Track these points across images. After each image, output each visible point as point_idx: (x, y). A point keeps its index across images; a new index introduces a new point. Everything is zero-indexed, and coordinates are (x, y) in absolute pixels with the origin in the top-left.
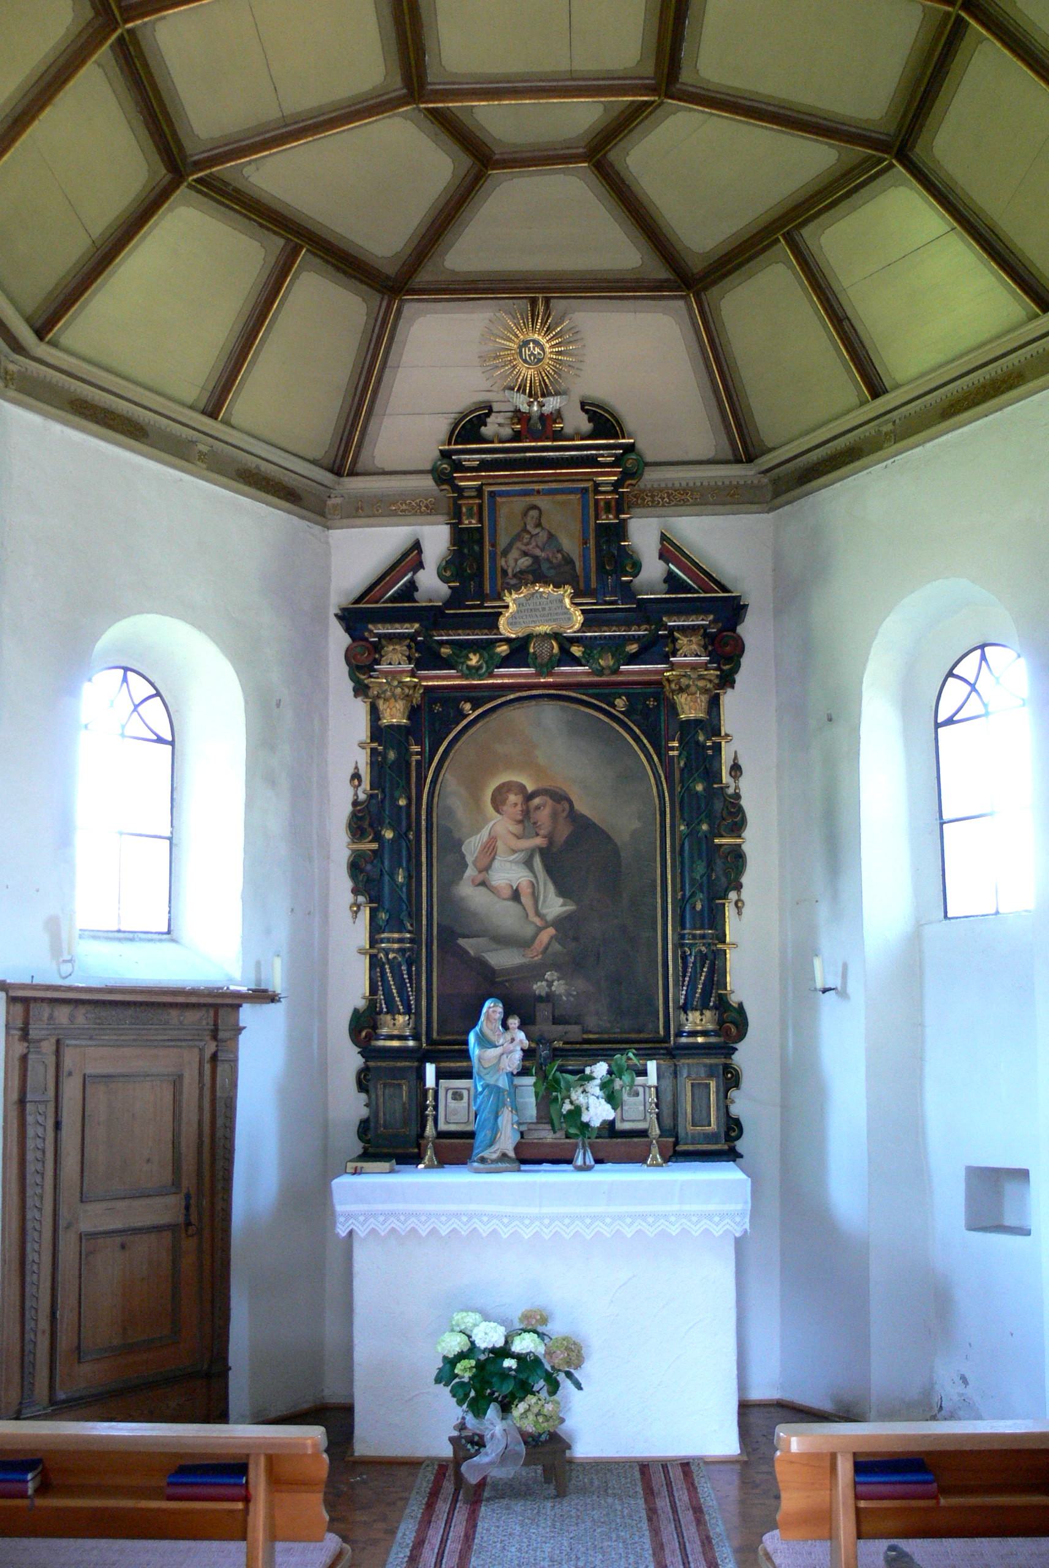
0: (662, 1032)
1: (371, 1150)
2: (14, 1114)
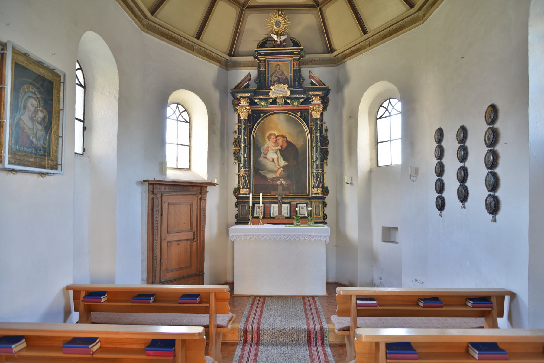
1: (238, 221)
2: (150, 211)
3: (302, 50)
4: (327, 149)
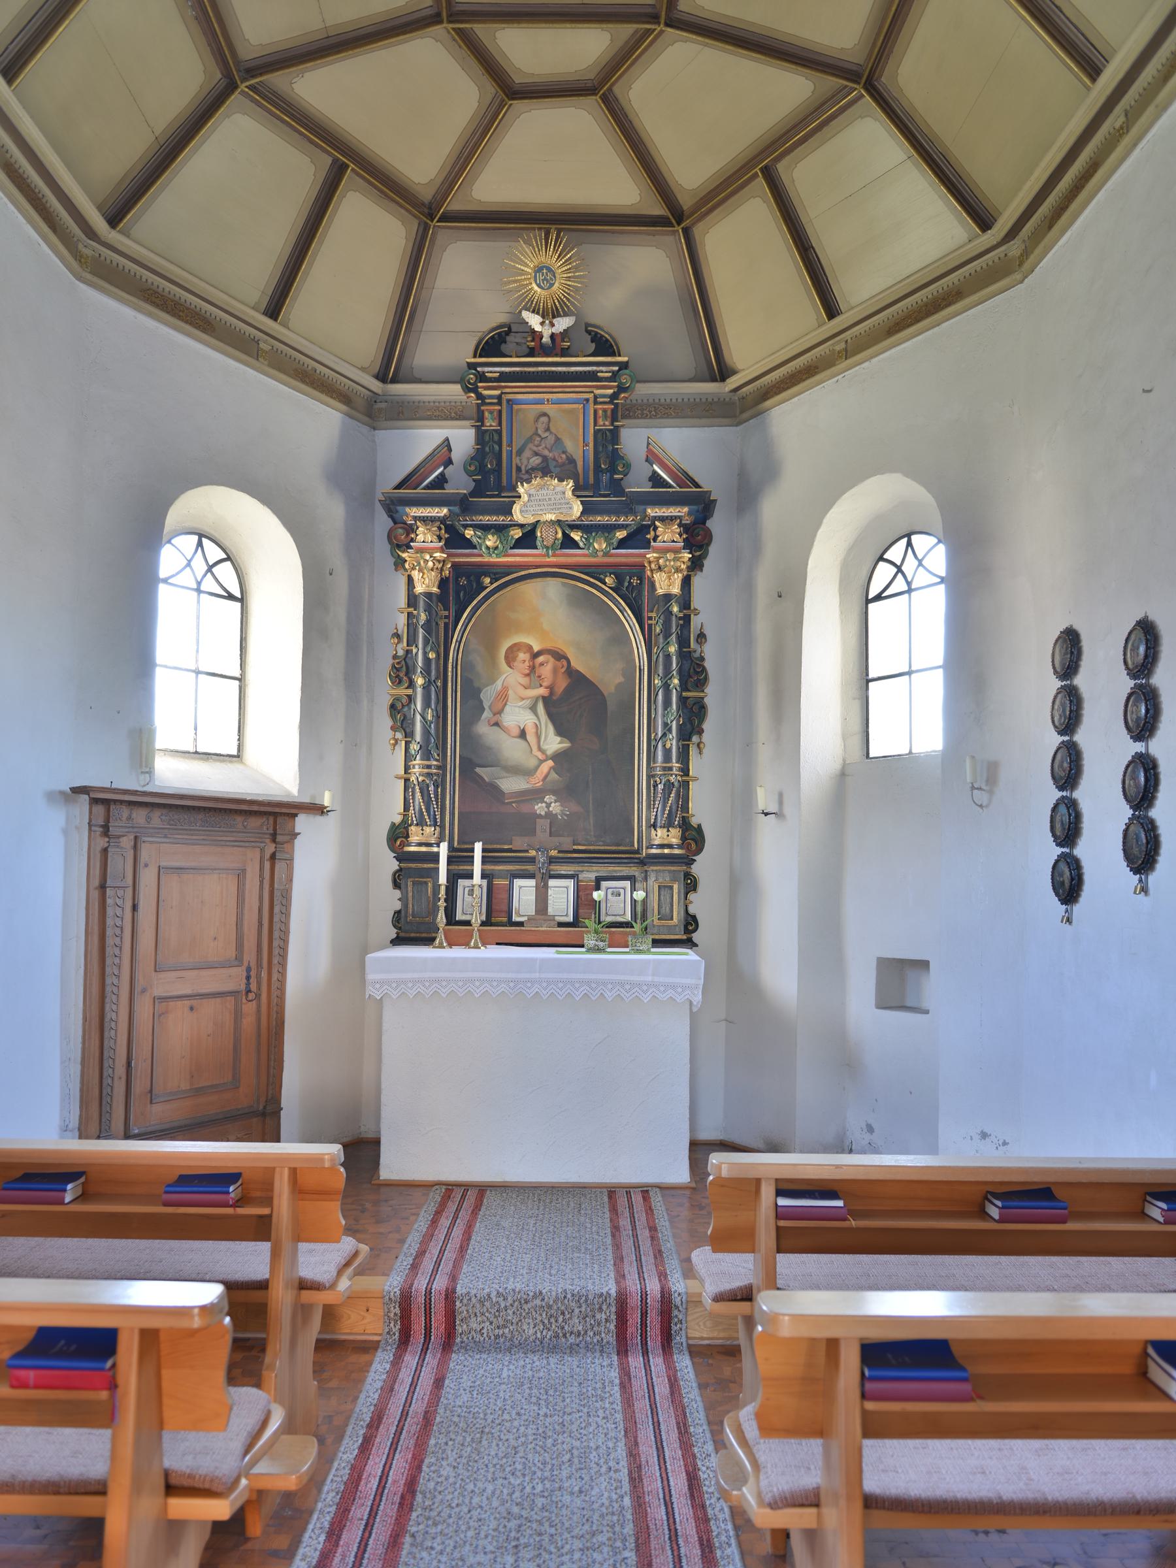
1: (402, 935)
2: (95, 894)
3: (624, 366)
4: (703, 698)
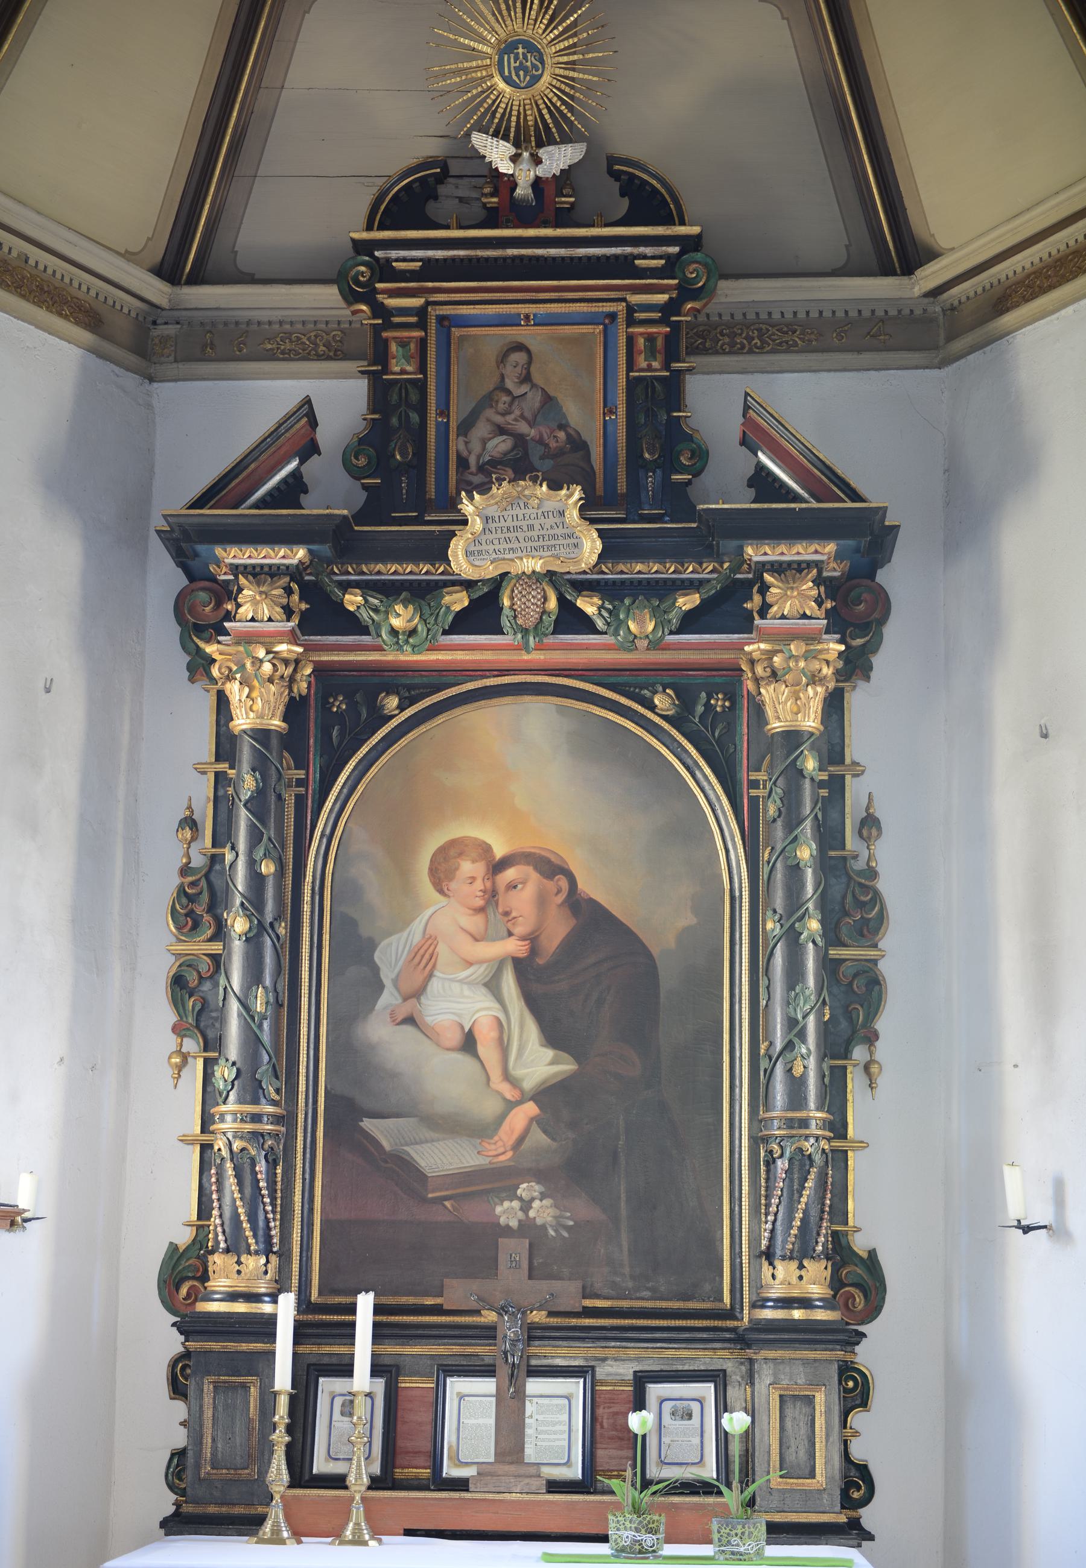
0: (727, 1299)
1: (187, 1509)
